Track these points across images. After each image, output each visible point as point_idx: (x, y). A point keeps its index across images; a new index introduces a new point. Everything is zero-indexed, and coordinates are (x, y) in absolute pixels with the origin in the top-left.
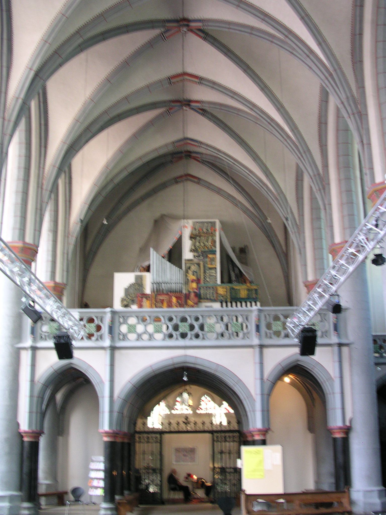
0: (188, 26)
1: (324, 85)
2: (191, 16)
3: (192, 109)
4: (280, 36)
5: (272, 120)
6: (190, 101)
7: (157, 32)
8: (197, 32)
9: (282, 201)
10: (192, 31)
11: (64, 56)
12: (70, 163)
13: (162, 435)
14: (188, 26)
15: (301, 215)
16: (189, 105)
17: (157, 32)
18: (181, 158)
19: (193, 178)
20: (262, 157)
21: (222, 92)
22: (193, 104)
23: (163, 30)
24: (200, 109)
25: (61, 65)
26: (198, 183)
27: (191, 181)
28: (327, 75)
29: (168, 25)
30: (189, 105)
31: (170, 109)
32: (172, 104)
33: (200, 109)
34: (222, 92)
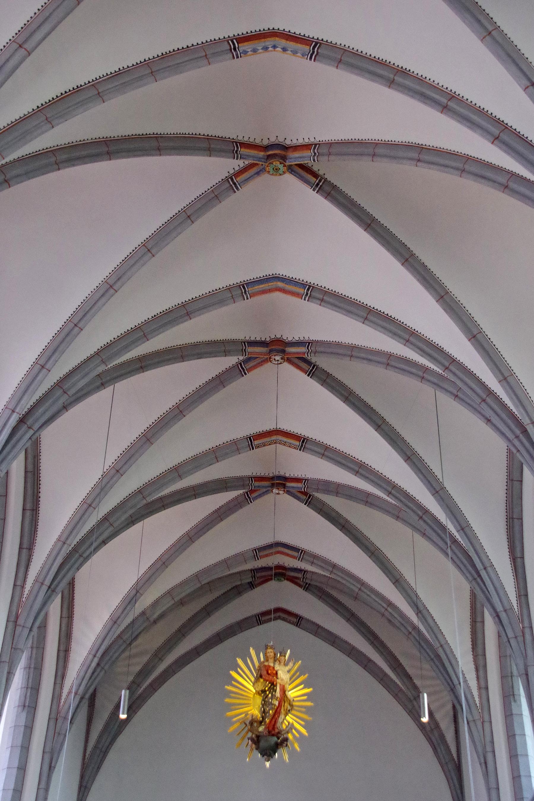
0: (283, 352)
1: (515, 451)
2: (289, 336)
3: (289, 493)
4: (436, 368)
5: (426, 511)
6: (286, 479)
7: (232, 360)
8: (296, 361)
9: (345, 579)
10: (289, 361)
11: (71, 392)
12: (73, 579)
13: (312, 296)
14: (283, 352)
15: (484, 688)
16: (284, 486)
17: (232, 360)
18: (267, 580)
19: (287, 437)
20: (408, 575)
21: (404, 370)
22: (289, 484)
23: (241, 358)
24: (301, 492)
25: (65, 408)
26: (297, 625)
27: (284, 619)
28: (518, 432)
29: (250, 349)
30: (284, 486)
31: (252, 491)
32: (257, 484)
33: (301, 492)
34: (404, 370)
